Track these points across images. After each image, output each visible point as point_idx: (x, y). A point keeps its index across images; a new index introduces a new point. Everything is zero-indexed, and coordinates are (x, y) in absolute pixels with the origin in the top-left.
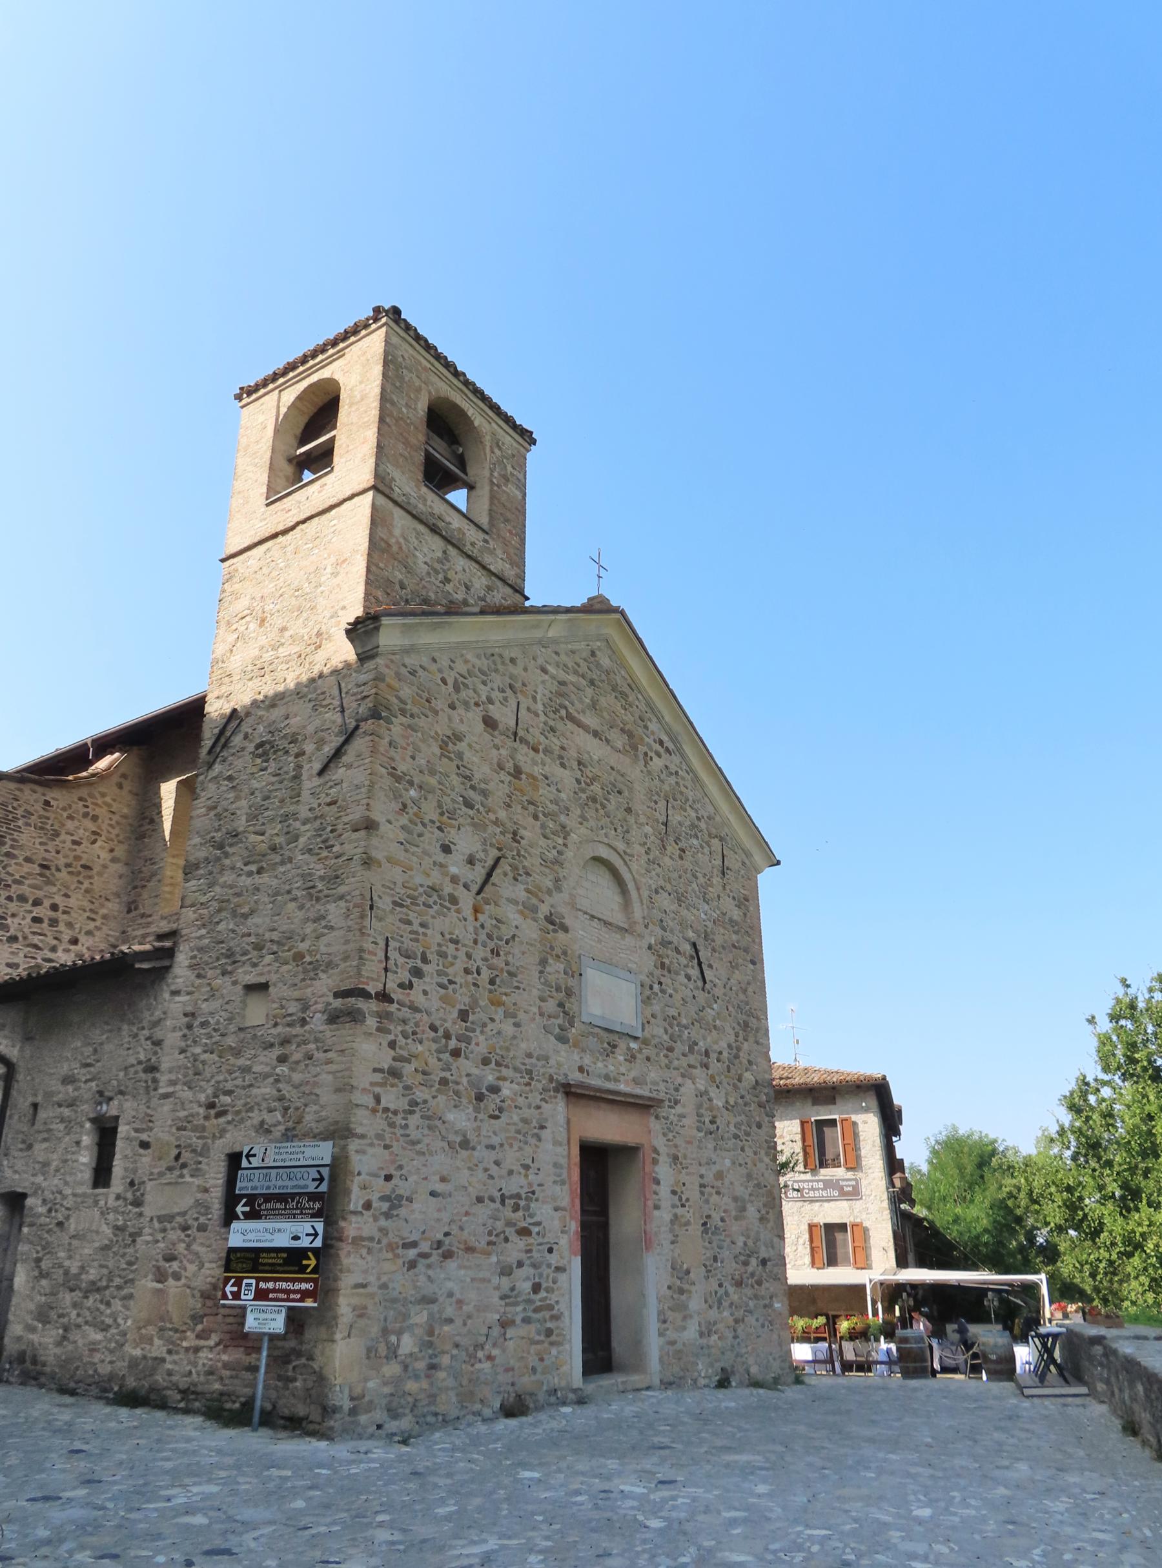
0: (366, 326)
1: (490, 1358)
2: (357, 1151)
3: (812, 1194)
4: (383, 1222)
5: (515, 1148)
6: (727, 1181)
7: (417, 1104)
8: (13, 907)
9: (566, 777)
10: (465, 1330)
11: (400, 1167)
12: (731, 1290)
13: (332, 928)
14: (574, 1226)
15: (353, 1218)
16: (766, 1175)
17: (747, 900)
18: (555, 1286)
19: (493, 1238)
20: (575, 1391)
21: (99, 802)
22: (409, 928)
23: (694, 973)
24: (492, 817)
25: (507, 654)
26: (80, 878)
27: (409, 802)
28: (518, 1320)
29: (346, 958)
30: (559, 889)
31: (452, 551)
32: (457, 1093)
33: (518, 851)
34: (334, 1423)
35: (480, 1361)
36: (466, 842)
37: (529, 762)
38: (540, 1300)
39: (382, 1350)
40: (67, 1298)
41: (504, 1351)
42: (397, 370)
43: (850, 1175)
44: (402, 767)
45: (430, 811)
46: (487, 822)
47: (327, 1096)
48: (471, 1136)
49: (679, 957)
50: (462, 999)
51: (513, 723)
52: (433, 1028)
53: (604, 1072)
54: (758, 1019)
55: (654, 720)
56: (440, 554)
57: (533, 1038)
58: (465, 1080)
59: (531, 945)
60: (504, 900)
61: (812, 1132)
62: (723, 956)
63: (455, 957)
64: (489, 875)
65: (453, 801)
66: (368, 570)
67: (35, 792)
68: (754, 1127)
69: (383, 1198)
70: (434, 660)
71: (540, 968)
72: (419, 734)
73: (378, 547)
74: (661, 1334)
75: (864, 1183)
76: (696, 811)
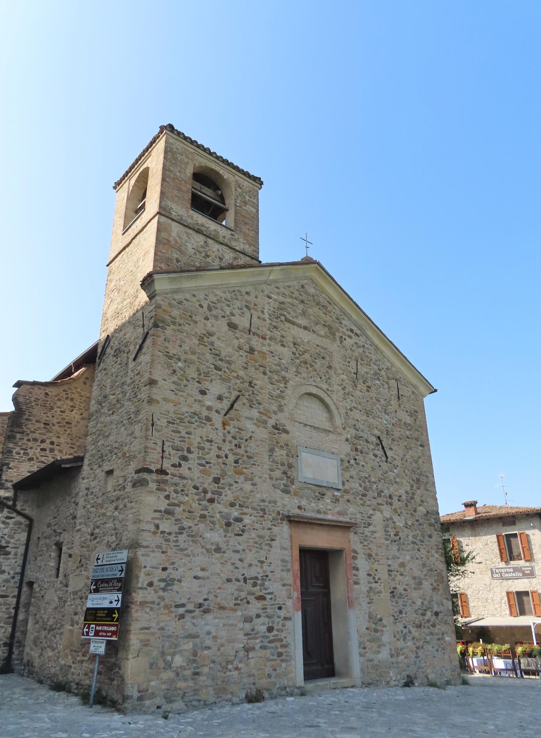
0: (158, 137)
1: (237, 669)
2: (143, 555)
3: (507, 575)
4: (161, 593)
5: (254, 551)
6: (407, 568)
7: (184, 529)
8: (30, 444)
9: (286, 353)
10: (219, 653)
11: (173, 563)
12: (413, 630)
13: (135, 438)
14: (296, 594)
15: (141, 592)
16: (437, 564)
17: (417, 412)
18: (284, 628)
19: (239, 602)
20: (299, 688)
21: (74, 391)
22: (178, 435)
23: (380, 453)
24: (235, 374)
25: (243, 290)
26: (66, 429)
27: (178, 369)
28: (257, 647)
29: (140, 453)
30: (282, 411)
31: (210, 241)
32: (213, 523)
33: (253, 392)
34: (128, 705)
35: (230, 671)
36: (216, 388)
37: (259, 345)
38: (273, 636)
39: (161, 664)
40: (44, 633)
41: (247, 665)
42: (173, 155)
43: (528, 564)
44: (172, 352)
45: (192, 373)
46: (231, 377)
47: (131, 527)
48: (223, 546)
49: (368, 444)
50: (216, 472)
51: (248, 325)
52: (196, 488)
53: (316, 509)
54: (427, 477)
55: (346, 318)
56: (202, 243)
57: (265, 491)
58: (218, 515)
59: (263, 441)
60: (243, 418)
61: (504, 542)
62: (400, 443)
63: (210, 449)
64: (232, 406)
65: (208, 367)
66: (155, 254)
67: (40, 389)
68: (427, 537)
69: (160, 580)
70: (194, 296)
71: (269, 453)
72: (185, 334)
73: (161, 241)
74: (361, 655)
75: (536, 568)
76: (378, 366)
